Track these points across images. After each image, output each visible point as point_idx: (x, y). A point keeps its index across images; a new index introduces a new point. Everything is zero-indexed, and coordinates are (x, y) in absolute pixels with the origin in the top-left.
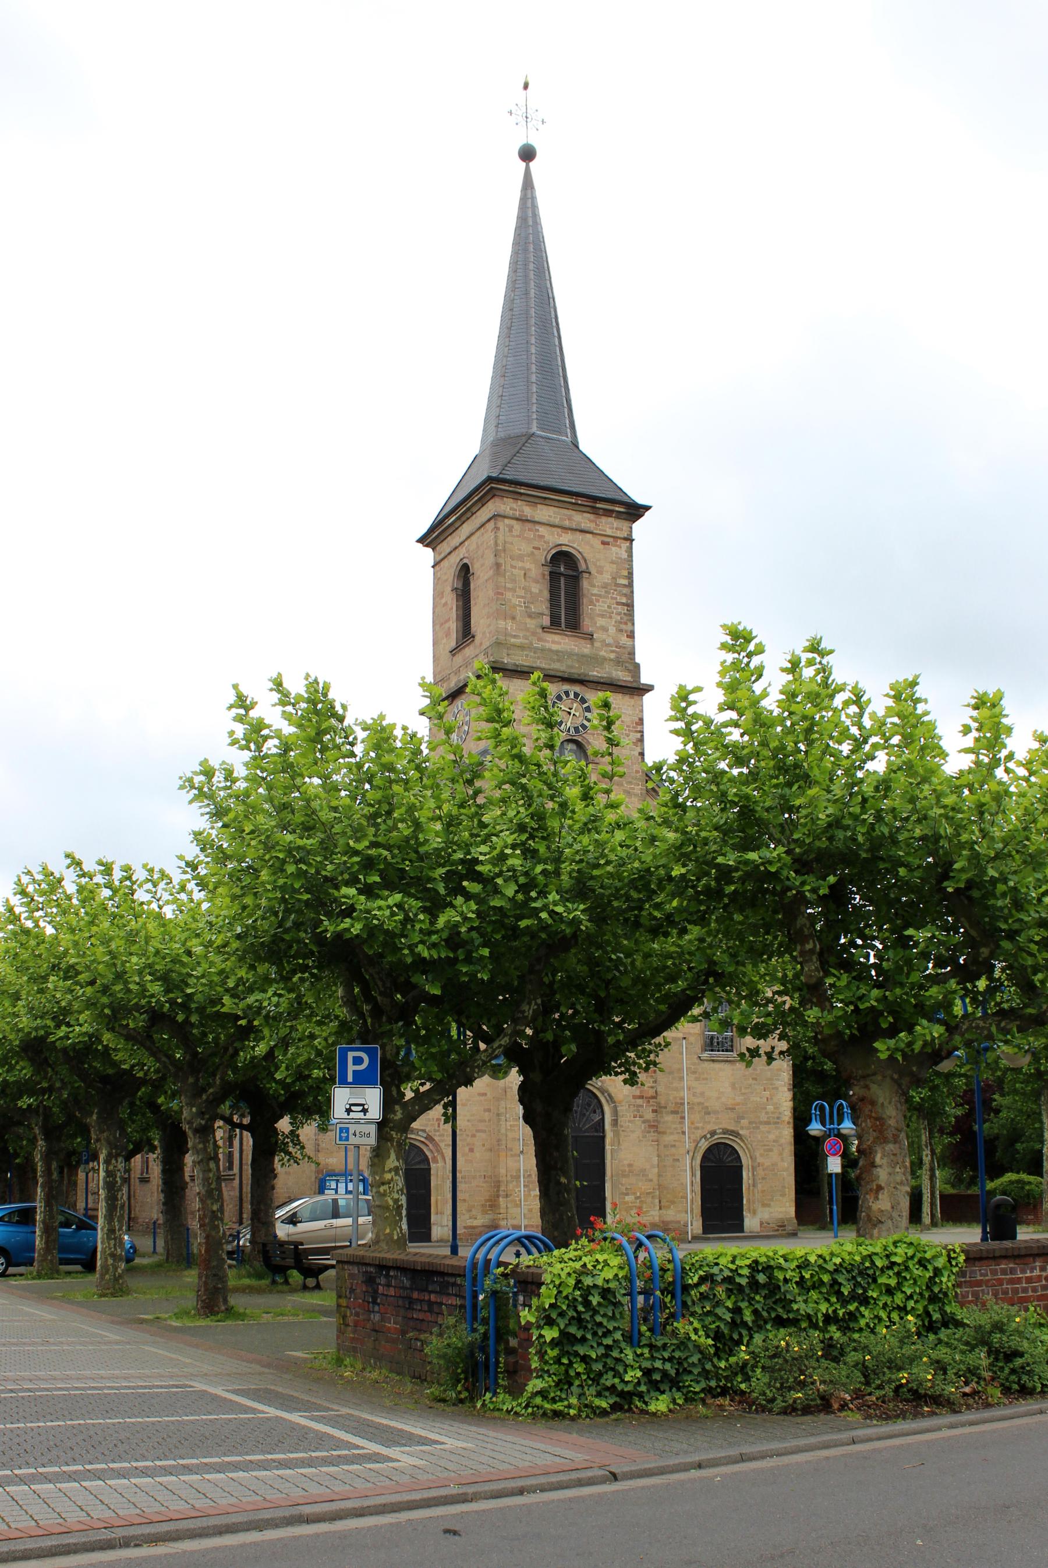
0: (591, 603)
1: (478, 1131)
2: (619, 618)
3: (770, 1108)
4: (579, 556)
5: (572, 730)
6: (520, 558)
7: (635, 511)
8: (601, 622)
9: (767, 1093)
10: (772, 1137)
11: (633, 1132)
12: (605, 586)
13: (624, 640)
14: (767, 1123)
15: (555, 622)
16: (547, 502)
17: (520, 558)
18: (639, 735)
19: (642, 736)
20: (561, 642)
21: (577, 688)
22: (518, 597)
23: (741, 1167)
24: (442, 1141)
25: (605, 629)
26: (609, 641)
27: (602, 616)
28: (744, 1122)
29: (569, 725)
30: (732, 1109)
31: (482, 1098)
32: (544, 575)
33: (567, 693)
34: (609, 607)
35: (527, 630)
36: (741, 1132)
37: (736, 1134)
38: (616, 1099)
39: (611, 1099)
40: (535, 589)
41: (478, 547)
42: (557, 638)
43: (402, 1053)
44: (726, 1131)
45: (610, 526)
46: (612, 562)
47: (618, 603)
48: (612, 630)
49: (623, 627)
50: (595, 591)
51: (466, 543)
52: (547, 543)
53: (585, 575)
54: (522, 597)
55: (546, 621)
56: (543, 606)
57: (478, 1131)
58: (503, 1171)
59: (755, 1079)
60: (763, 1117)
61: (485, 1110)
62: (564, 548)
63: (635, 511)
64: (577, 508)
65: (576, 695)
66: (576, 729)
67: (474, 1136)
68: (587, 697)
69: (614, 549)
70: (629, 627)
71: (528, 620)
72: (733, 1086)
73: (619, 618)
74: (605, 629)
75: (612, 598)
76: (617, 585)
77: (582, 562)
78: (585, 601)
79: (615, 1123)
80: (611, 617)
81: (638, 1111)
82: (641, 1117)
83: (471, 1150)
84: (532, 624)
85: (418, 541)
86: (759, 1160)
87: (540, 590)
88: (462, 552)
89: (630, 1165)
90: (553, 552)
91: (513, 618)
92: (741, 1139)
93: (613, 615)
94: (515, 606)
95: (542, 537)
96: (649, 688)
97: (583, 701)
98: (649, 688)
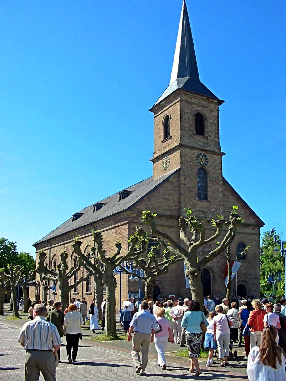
0: (207, 128)
1: (175, 280)
2: (215, 133)
3: (255, 274)
4: (204, 115)
5: (202, 165)
6: (187, 113)
7: (220, 102)
8: (210, 134)
9: (254, 270)
10: (255, 282)
11: (219, 281)
12: (211, 123)
13: (216, 139)
14: (254, 278)
15: (197, 133)
16: (195, 97)
17: (187, 113)
18: (221, 167)
19: (222, 168)
20: (198, 138)
21: (204, 153)
22: (187, 125)
23: (246, 291)
24: (164, 283)
25: (211, 136)
26: (212, 139)
27: (210, 132)
28: (248, 278)
29: (201, 163)
30: (244, 275)
31: (176, 271)
32: (194, 119)
33: (201, 154)
34: (212, 130)
35: (189, 134)
36: (247, 281)
37: (245, 281)
38: (214, 272)
39: (213, 271)
40: (191, 123)
41: (172, 110)
42: (198, 138)
43: (166, 299)
44: (243, 281)
45: (212, 106)
46: (213, 117)
47: (215, 129)
48: (213, 136)
49: (216, 136)
50: (208, 125)
51: (168, 110)
52: (195, 109)
53: (206, 120)
54: (188, 125)
55: (195, 132)
56: (193, 128)
57: (175, 280)
58: (182, 292)
59: (251, 266)
60: (253, 277)
61: (177, 275)
62: (200, 112)
63: (220, 102)
64: (203, 100)
65: (203, 155)
66: (204, 165)
67: (173, 282)
68: (207, 155)
69: (213, 113)
70: (218, 136)
71: (189, 132)
72: (245, 268)
73: (215, 133)
74: (211, 136)
75: (213, 127)
76: (215, 124)
77: (205, 116)
78: (205, 127)
79: (214, 278)
80: (213, 133)
81: (220, 275)
82: (221, 276)
83: (172, 286)
84: (190, 133)
85: (34, 246)
86: (251, 289)
87: (193, 123)
88: (166, 112)
89: (218, 290)
90: (196, 112)
91: (185, 131)
92: (247, 283)
93: (213, 132)
94: (185, 127)
95: (193, 108)
96: (224, 154)
97: (205, 156)
98: (224, 154)
